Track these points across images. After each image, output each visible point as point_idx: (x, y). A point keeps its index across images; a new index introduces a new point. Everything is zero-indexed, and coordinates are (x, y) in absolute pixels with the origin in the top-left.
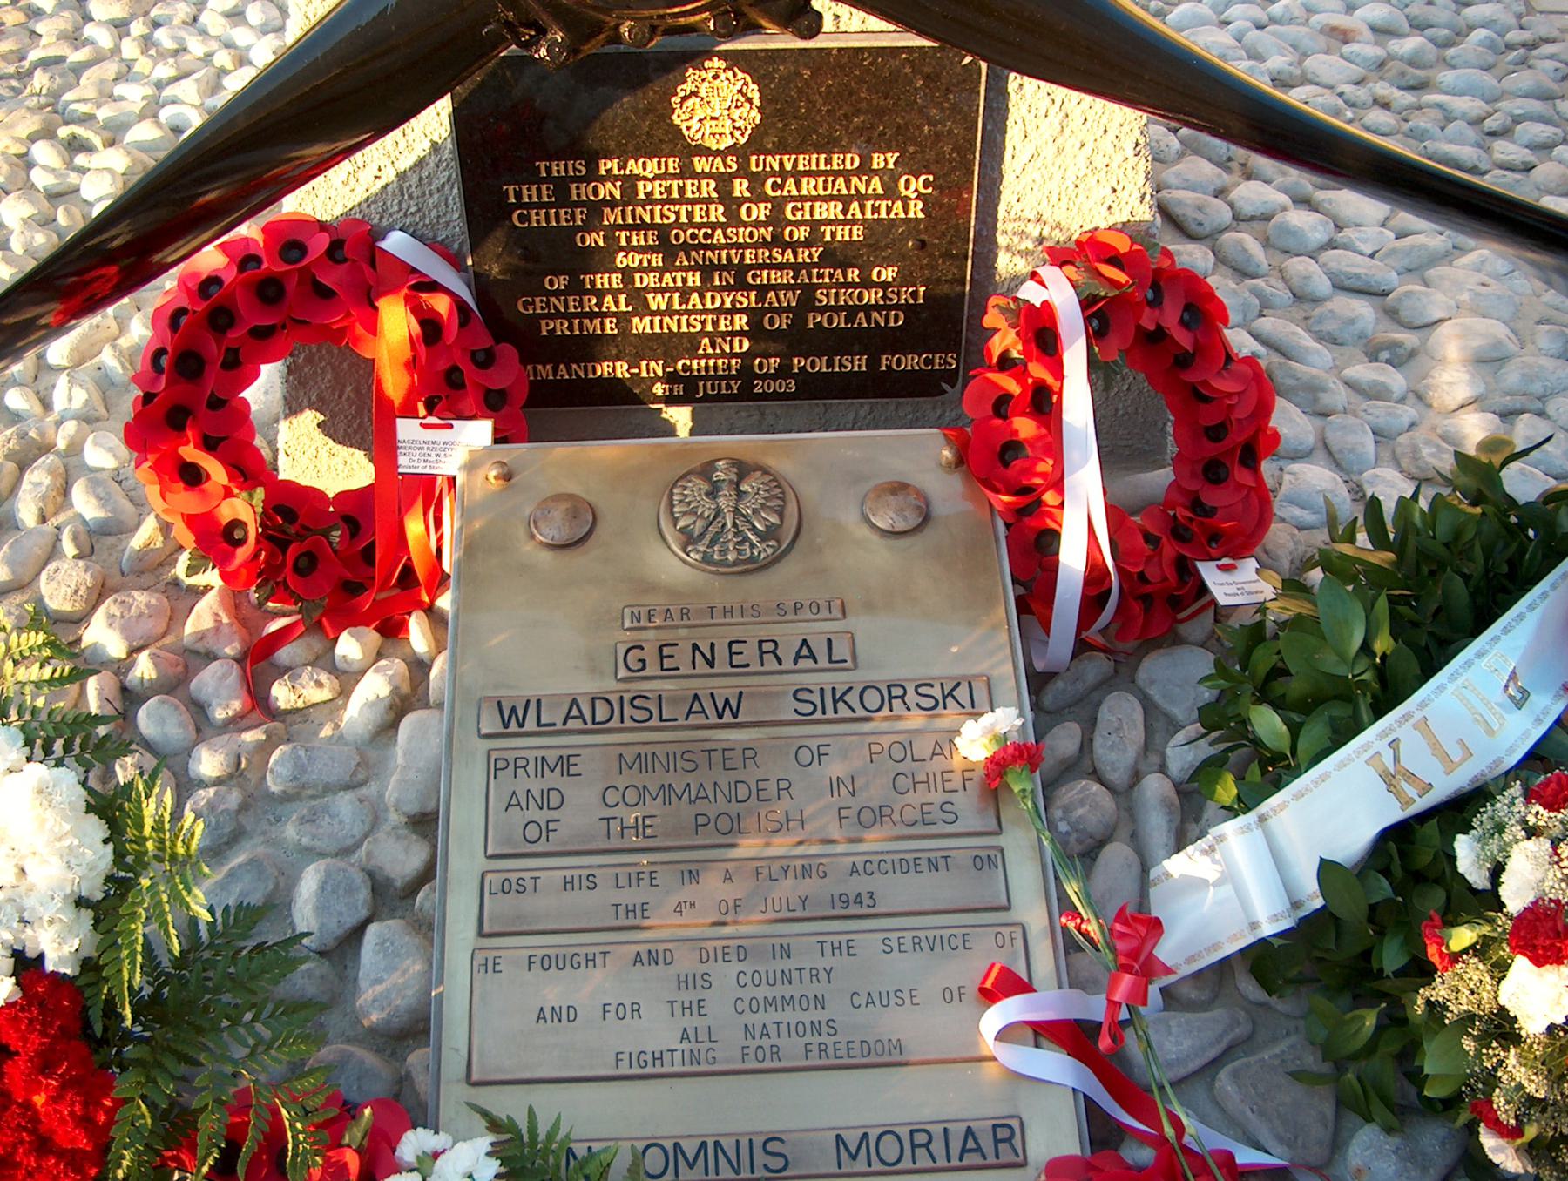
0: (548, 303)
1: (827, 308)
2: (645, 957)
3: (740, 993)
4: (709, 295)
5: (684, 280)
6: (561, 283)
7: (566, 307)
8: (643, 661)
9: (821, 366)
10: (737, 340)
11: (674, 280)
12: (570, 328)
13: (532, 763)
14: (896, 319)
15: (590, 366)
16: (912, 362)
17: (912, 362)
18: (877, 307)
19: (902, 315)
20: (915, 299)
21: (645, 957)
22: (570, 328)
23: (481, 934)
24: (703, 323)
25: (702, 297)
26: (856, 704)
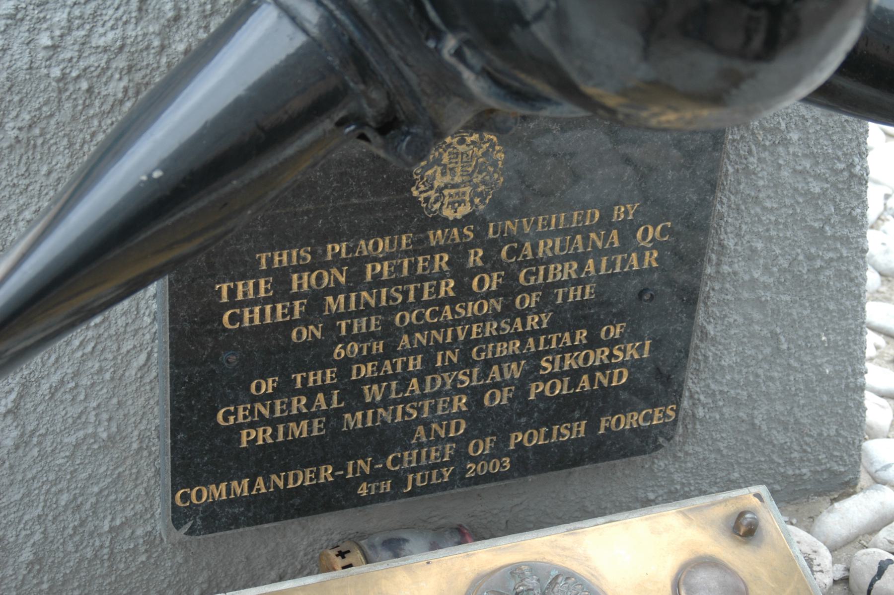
0: (252, 412)
1: (552, 375)
5: (405, 365)
6: (268, 386)
7: (272, 411)
9: (539, 439)
11: (394, 366)
12: (274, 436)
15: (291, 474)
18: (603, 368)
24: (420, 410)
25: (422, 382)
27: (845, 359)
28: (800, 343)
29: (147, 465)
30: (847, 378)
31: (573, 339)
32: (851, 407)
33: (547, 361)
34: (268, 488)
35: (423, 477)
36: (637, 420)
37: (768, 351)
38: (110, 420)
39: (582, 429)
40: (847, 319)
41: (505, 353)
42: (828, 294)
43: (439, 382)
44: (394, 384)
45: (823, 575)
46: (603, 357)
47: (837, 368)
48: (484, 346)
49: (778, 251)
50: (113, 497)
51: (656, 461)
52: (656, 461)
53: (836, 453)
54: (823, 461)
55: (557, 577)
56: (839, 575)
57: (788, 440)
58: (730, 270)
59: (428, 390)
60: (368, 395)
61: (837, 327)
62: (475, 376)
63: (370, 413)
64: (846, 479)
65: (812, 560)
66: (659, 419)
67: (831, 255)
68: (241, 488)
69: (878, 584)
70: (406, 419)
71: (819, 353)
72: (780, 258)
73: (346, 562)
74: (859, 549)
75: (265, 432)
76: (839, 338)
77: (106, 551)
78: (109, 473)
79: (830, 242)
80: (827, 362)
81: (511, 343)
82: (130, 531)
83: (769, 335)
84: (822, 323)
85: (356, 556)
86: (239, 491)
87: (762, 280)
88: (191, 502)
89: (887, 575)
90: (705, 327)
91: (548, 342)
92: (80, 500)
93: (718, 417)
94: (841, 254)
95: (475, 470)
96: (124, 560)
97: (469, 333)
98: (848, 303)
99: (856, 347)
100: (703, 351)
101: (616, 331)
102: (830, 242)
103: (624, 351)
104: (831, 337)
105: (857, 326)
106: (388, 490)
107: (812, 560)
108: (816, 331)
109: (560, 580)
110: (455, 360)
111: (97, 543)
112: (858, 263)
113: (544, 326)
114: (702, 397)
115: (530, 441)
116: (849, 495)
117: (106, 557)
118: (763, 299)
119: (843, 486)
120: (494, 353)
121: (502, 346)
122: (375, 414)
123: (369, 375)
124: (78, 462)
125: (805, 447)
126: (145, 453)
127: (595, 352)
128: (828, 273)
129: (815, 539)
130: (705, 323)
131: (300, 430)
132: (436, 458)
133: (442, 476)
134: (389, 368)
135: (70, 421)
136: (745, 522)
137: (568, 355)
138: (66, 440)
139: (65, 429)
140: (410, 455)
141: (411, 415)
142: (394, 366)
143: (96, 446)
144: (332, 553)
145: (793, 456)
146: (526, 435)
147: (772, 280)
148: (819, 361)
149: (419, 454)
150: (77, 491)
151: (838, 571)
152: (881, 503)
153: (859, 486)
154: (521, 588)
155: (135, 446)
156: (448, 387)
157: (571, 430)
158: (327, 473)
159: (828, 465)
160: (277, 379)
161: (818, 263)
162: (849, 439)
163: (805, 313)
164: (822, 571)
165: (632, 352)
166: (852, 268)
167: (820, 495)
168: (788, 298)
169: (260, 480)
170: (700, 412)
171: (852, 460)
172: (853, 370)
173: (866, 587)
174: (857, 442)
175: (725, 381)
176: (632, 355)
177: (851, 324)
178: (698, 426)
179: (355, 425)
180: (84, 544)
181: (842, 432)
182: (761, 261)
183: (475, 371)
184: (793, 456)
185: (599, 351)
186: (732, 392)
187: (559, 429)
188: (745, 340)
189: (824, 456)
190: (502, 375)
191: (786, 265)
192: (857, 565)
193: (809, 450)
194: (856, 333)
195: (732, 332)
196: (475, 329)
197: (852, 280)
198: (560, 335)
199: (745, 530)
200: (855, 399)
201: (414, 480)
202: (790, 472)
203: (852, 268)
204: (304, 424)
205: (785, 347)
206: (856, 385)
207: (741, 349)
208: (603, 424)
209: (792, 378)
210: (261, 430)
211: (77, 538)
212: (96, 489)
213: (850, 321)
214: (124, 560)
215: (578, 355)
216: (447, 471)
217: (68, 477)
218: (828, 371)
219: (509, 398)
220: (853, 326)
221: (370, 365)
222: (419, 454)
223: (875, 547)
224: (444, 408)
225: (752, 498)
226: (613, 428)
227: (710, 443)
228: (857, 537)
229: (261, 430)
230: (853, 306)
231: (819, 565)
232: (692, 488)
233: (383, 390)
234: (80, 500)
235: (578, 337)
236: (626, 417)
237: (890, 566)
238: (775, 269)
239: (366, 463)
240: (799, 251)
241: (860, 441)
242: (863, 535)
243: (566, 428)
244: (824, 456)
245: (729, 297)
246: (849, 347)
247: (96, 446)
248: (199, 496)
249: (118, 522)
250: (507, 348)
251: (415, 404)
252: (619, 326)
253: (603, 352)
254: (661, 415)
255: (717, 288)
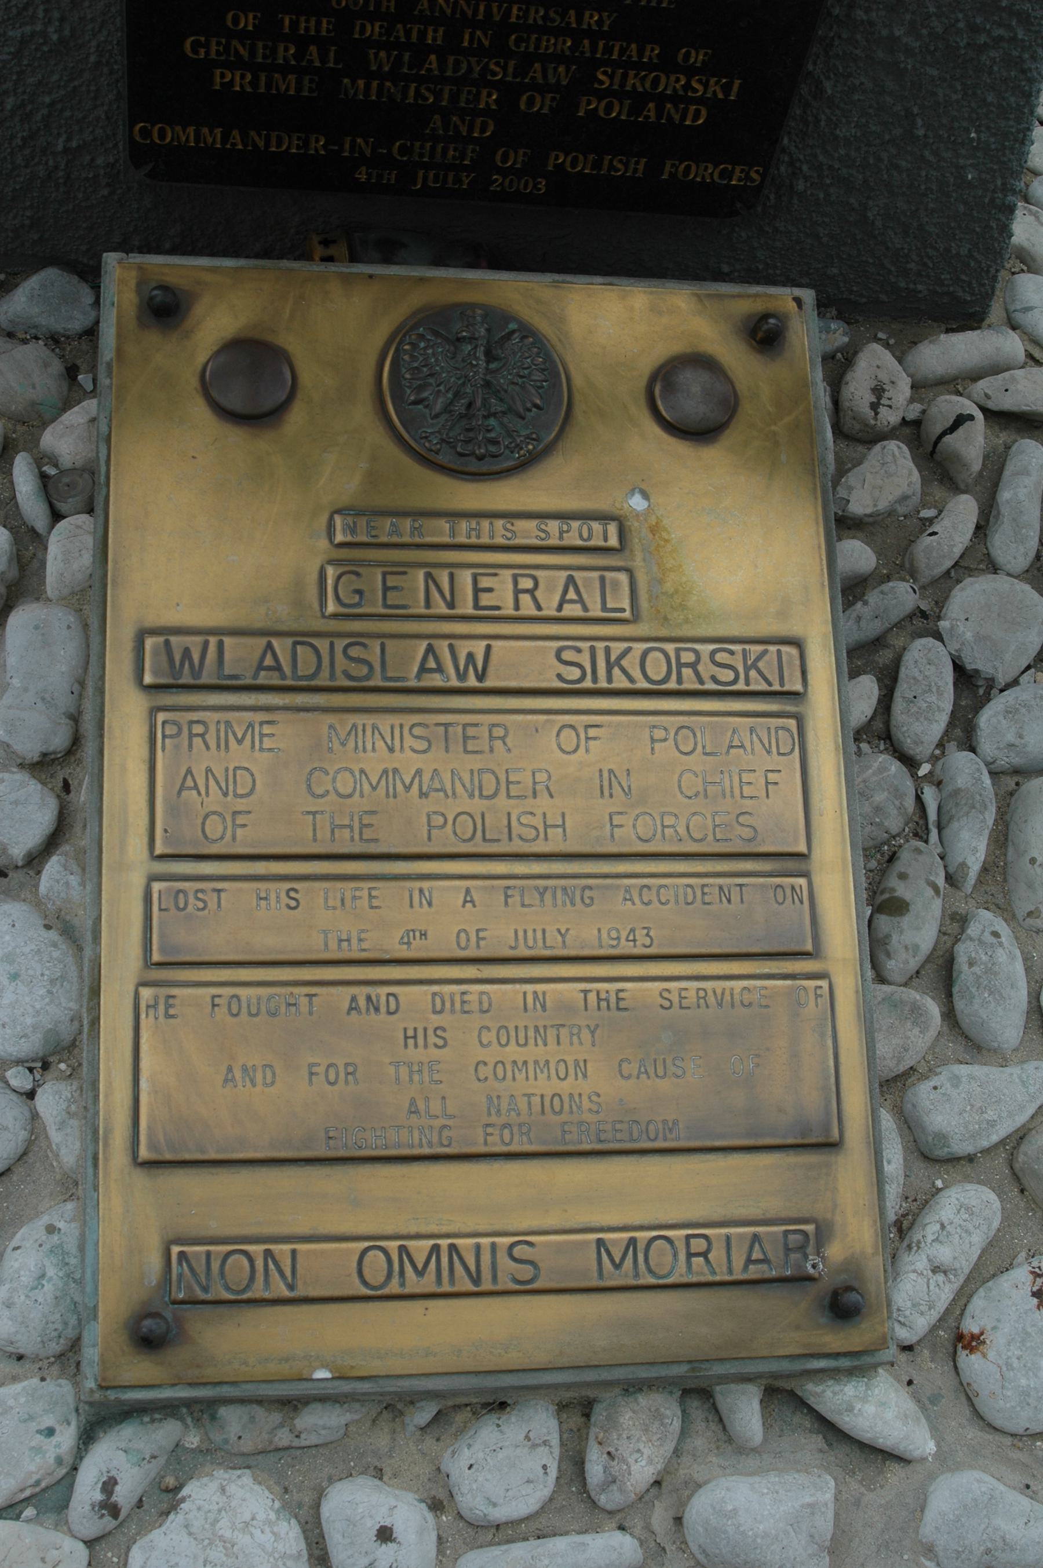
0: (227, 48)
1: (609, 93)
2: (362, 1002)
3: (482, 1054)
4: (451, 59)
5: (423, 35)
6: (248, 21)
7: (253, 53)
8: (359, 592)
9: (584, 166)
10: (479, 121)
11: (408, 33)
12: (254, 83)
13: (212, 728)
14: (697, 115)
15: (274, 135)
16: (706, 173)
17: (706, 173)
18: (675, 99)
19: (704, 112)
20: (727, 93)
21: (362, 1002)
22: (254, 83)
23: (149, 964)
24: (438, 95)
25: (442, 62)
26: (637, 673)
27: (995, 167)
28: (941, 133)
29: (108, 85)
30: (994, 191)
31: (641, 53)
32: (992, 228)
33: (605, 73)
34: (245, 145)
35: (436, 176)
36: (712, 174)
37: (897, 132)
38: (62, 19)
39: (641, 167)
40: (1008, 119)
41: (551, 51)
42: (988, 81)
43: (464, 66)
44: (406, 56)
45: (890, 411)
46: (678, 86)
47: (984, 176)
48: (525, 35)
49: (932, 9)
50: (68, 113)
51: (737, 229)
52: (737, 229)
53: (963, 277)
54: (946, 282)
55: (513, 332)
56: (911, 416)
57: (906, 246)
58: (865, 18)
59: (449, 73)
60: (373, 60)
61: (993, 126)
62: (510, 70)
63: (375, 84)
64: (971, 311)
65: (884, 390)
66: (740, 180)
67: (1001, 32)
68: (213, 137)
69: (948, 438)
70: (420, 102)
71: (963, 152)
72: (934, 18)
73: (330, 251)
74: (950, 393)
75: (243, 77)
76: (992, 140)
77: (61, 174)
78: (62, 84)
79: (1004, 15)
80: (971, 165)
81: (561, 39)
82: (88, 158)
83: (903, 113)
84: (974, 116)
85: (341, 249)
86: (210, 140)
87: (905, 40)
88: (152, 140)
89: (961, 431)
90: (821, 82)
91: (608, 50)
92: (29, 108)
93: (822, 196)
94: (1016, 34)
95: (501, 184)
96: (82, 189)
97: (508, 13)
98: (1012, 99)
99: (1012, 157)
100: (814, 111)
101: (698, 58)
102: (1004, 15)
103: (706, 86)
104: (982, 135)
105: (1019, 131)
106: (393, 182)
107: (884, 390)
108: (965, 124)
109: (516, 335)
110: (486, 43)
111: (51, 163)
112: (1035, 52)
113: (606, 28)
114: (805, 168)
115: (573, 166)
116: (973, 329)
117: (61, 181)
118: (902, 66)
119: (968, 317)
120: (537, 47)
121: (548, 41)
122: (381, 87)
123: (376, 37)
124: (25, 62)
125: (926, 260)
126: (105, 70)
127: (668, 78)
128: (993, 54)
129: (900, 368)
130: (822, 77)
131: (288, 86)
132: (454, 157)
133: (461, 182)
134: (402, 33)
135: (14, 11)
136: (765, 327)
137: (632, 73)
138: (10, 33)
139: (9, 19)
140: (422, 147)
141: (427, 99)
142: (408, 33)
143: (45, 49)
144: (316, 239)
145: (909, 266)
146: (569, 159)
147: (918, 44)
148: (961, 161)
149: (433, 149)
150: (26, 97)
151: (913, 412)
152: (997, 348)
153: (987, 322)
154: (464, 334)
155: (93, 59)
156: (476, 75)
157: (626, 165)
158: (318, 144)
159: (951, 289)
160: (259, 15)
161: (982, 39)
162: (984, 265)
163: (954, 97)
164: (890, 407)
165: (715, 88)
166: (1026, 56)
167: (935, 321)
168: (935, 73)
169: (235, 133)
170: (801, 186)
171: (982, 290)
172: (1004, 184)
173: (934, 439)
174: (992, 271)
175: (836, 155)
176: (715, 93)
177: (1012, 127)
178: (796, 201)
179: (356, 94)
180: (36, 160)
181: (975, 254)
182: (908, 17)
183: (512, 63)
184: (909, 266)
185: (673, 78)
186: (845, 171)
187: (611, 161)
188: (871, 111)
189: (948, 277)
190: (545, 76)
191: (939, 30)
192: (933, 410)
193: (931, 265)
194: (1016, 140)
195: (856, 97)
196: (515, 11)
197: (1023, 71)
198: (625, 44)
199: (765, 336)
200: (999, 220)
201: (425, 178)
202: (903, 285)
203: (1026, 56)
204: (292, 78)
205: (921, 132)
206: (1004, 204)
207: (864, 121)
208: (668, 168)
209: (924, 174)
210: (238, 73)
211: (27, 152)
212: (47, 100)
213: (1011, 123)
214: (82, 189)
215: (646, 76)
216: (467, 177)
217: (14, 77)
218: (970, 177)
219: (551, 108)
220: (1014, 130)
221: (377, 24)
222: (433, 149)
223: (969, 398)
224: (467, 99)
225: (792, 303)
226: (680, 175)
227: (808, 224)
228: (955, 378)
229: (238, 73)
230: (1018, 105)
231: (889, 399)
232: (778, 272)
233: (392, 59)
234: (29, 108)
235: (647, 53)
236: (698, 167)
237: (969, 423)
238: (924, 32)
239: (367, 143)
240: (960, 16)
241: (997, 271)
242: (963, 379)
243: (621, 161)
244: (948, 277)
245: (857, 52)
246: (1004, 155)
247: (45, 49)
248: (162, 135)
249: (74, 144)
250: (555, 44)
251: (432, 86)
252: (702, 52)
253: (678, 80)
254: (743, 175)
255: (844, 36)
